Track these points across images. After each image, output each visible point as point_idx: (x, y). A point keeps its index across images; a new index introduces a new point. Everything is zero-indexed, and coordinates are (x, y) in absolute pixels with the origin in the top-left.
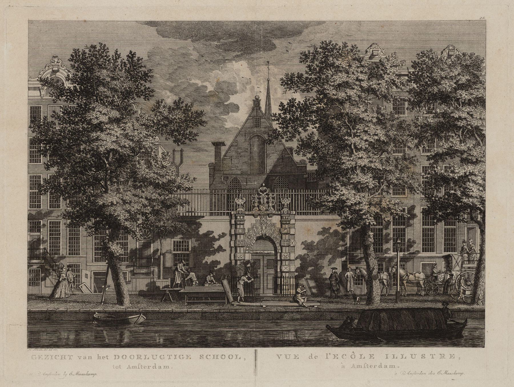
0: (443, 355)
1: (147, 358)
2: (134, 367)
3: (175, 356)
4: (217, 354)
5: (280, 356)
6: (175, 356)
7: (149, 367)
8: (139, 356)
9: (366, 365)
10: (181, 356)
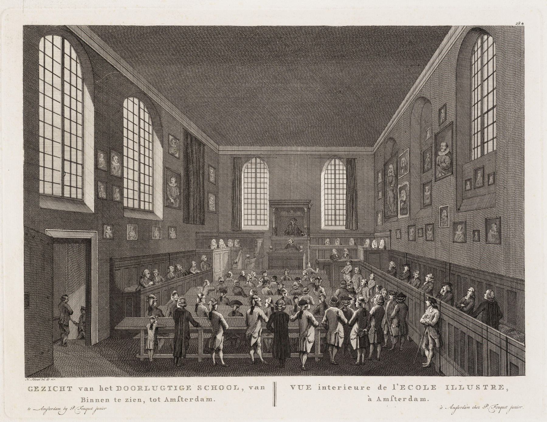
0: (140, 387)
1: (462, 388)
2: (172, 400)
3: (176, 387)
4: (216, 385)
5: (81, 388)
6: (176, 387)
7: (404, 399)
8: (494, 386)
9: (180, 398)
10: (163, 388)
